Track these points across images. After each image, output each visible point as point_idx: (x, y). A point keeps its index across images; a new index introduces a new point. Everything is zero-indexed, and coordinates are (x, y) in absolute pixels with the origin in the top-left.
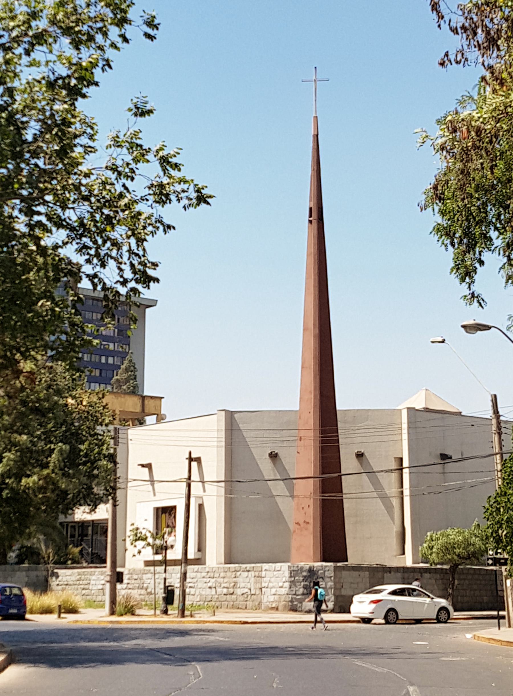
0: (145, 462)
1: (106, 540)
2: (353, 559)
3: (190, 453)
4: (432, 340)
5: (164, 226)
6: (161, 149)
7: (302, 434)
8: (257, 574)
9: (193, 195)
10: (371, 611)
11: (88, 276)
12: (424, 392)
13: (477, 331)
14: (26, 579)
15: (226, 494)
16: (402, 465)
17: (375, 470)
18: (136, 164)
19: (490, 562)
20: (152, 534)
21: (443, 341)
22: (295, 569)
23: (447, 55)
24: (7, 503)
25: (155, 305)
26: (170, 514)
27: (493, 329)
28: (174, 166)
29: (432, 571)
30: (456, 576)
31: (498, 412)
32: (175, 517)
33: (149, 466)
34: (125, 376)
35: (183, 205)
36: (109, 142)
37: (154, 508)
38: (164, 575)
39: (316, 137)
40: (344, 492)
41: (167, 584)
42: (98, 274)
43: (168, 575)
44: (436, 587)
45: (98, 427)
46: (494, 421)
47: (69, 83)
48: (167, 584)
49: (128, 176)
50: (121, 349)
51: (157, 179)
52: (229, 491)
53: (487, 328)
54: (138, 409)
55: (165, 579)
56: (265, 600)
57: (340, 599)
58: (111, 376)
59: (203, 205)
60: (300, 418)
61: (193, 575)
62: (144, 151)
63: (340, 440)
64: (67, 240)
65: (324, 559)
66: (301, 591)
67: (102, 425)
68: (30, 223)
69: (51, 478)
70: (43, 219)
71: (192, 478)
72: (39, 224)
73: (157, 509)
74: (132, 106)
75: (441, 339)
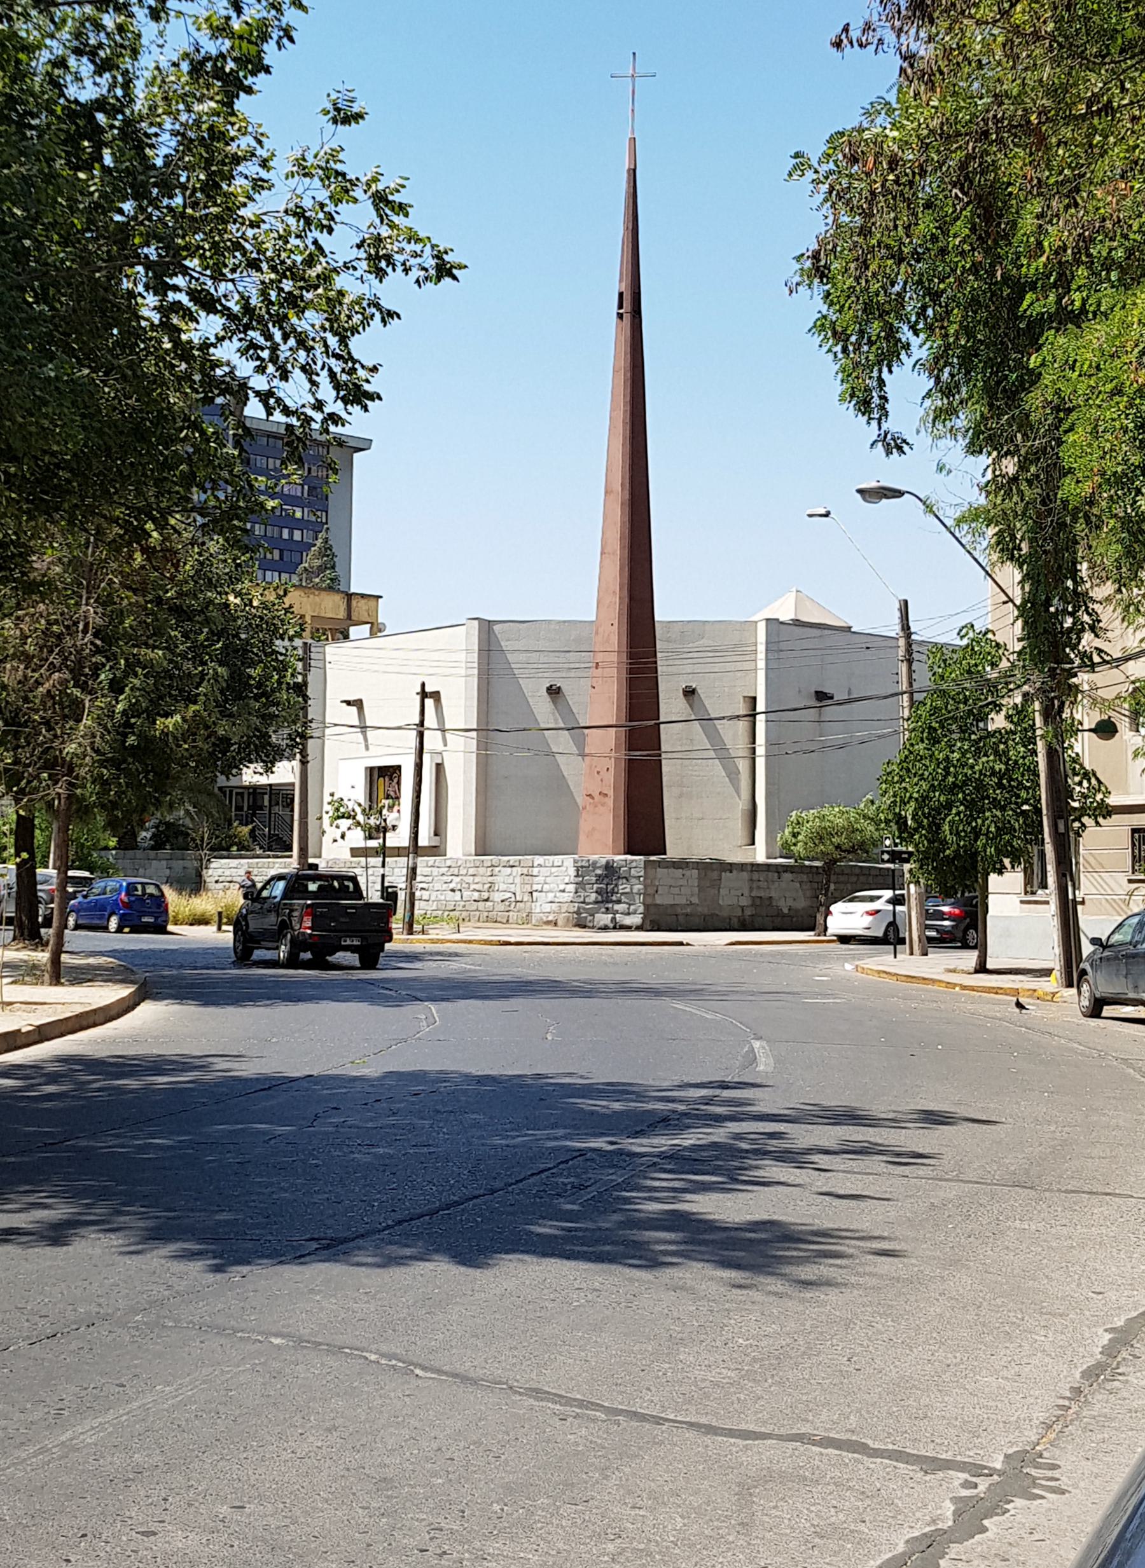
0: (351, 697)
1: (292, 816)
2: (674, 849)
3: (423, 685)
4: (810, 512)
5: (381, 312)
6: (375, 180)
7: (600, 658)
8: (525, 871)
9: (430, 263)
10: (866, 925)
11: (258, 394)
12: (794, 594)
13: (881, 498)
14: (168, 872)
15: (478, 749)
16: (755, 709)
17: (713, 716)
18: (336, 206)
19: (886, 857)
20: (364, 811)
21: (827, 515)
22: (584, 864)
23: (846, 29)
24: (133, 756)
25: (369, 448)
26: (391, 779)
27: (906, 495)
28: (397, 209)
29: (796, 870)
30: (833, 878)
31: (909, 628)
32: (399, 783)
33: (358, 704)
34: (317, 563)
35: (414, 279)
36: (290, 168)
37: (366, 768)
38: (381, 871)
39: (633, 173)
40: (663, 749)
41: (386, 884)
42: (275, 390)
43: (387, 871)
44: (800, 893)
45: (278, 642)
46: (902, 642)
47: (223, 68)
48: (386, 884)
49: (323, 226)
50: (313, 519)
51: (372, 230)
52: (483, 745)
53: (897, 494)
54: (342, 614)
55: (383, 876)
56: (538, 910)
57: (652, 910)
58: (298, 560)
59: (447, 280)
60: (597, 633)
61: (427, 871)
62: (348, 184)
63: (659, 669)
64: (222, 333)
65: (630, 851)
66: (593, 896)
67: (283, 639)
68: (162, 306)
69: (202, 718)
70: (184, 299)
71: (426, 724)
72: (177, 306)
73: (371, 770)
74: (330, 107)
75: (823, 511)
